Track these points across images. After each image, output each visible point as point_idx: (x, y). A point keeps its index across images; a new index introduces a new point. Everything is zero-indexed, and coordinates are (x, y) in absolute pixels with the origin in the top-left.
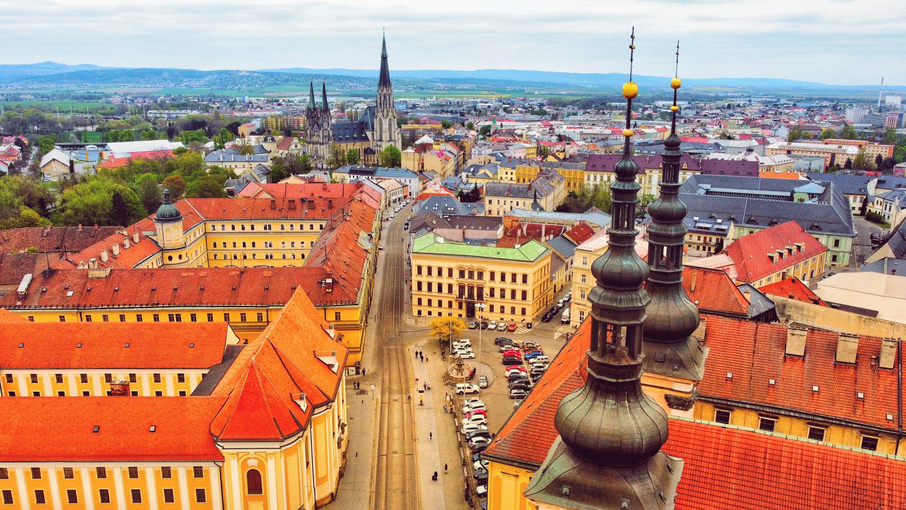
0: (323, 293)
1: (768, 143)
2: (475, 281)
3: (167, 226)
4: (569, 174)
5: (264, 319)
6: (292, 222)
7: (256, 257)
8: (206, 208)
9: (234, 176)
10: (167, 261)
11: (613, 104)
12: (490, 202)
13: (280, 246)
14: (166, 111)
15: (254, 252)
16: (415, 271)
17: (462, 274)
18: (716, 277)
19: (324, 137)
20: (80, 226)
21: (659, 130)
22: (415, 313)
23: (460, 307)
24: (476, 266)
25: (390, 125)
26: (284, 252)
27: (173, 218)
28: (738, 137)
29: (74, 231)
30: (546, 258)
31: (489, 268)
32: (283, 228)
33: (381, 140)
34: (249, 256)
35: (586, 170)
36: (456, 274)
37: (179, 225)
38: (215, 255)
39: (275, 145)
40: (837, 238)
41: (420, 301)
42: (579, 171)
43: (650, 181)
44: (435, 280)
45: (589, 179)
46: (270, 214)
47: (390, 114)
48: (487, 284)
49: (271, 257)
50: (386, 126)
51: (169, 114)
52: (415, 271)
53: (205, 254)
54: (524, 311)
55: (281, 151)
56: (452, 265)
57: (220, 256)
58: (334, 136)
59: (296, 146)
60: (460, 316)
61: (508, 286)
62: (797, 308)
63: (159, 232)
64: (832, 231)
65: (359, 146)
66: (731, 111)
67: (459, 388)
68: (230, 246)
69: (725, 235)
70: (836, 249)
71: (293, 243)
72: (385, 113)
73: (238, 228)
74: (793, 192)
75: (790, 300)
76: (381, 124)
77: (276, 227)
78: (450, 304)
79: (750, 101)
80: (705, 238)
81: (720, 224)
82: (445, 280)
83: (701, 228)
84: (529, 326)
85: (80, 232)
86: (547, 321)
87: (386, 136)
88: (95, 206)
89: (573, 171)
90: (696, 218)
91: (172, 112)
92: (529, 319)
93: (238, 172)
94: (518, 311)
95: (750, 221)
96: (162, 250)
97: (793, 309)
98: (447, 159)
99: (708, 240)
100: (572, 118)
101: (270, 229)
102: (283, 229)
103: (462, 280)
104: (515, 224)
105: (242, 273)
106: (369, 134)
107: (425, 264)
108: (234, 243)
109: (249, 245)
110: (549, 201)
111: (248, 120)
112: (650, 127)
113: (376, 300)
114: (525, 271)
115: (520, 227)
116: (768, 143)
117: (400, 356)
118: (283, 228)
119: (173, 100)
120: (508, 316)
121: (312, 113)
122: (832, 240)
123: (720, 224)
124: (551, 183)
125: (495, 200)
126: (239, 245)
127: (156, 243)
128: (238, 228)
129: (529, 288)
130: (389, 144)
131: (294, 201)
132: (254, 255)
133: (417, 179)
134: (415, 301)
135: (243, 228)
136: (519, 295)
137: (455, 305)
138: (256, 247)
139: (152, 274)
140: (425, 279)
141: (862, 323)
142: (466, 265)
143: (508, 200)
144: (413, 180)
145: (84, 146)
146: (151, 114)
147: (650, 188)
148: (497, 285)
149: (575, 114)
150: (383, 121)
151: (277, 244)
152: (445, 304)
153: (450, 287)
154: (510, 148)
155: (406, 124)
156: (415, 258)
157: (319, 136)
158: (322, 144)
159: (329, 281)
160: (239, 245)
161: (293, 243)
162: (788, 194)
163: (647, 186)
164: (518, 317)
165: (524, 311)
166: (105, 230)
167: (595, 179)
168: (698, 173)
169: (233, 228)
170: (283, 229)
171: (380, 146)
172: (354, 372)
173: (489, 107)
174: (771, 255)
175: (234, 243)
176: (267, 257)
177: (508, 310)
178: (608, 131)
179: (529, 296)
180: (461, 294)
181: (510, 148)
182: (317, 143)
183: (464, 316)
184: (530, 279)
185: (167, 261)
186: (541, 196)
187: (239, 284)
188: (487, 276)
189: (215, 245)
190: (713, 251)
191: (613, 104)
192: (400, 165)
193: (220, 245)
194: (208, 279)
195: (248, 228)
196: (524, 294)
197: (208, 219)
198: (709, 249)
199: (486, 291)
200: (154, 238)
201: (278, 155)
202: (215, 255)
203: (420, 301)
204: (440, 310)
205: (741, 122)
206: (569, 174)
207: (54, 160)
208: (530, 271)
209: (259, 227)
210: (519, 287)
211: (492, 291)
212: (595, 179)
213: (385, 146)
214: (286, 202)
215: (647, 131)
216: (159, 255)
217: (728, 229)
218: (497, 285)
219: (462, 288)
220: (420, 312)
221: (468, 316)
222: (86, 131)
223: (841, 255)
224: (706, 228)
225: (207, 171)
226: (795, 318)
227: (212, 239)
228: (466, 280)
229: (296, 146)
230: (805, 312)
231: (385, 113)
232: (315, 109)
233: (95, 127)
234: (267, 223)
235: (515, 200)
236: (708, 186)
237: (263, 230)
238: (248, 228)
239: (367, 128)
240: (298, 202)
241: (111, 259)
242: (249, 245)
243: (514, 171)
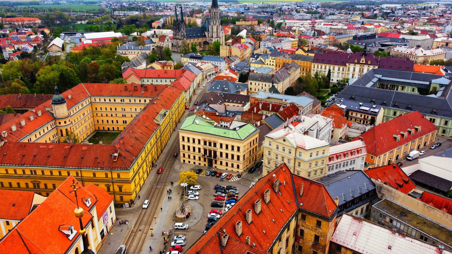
0: (111, 162)
1: (437, 37)
2: (212, 148)
3: (56, 106)
4: (304, 64)
5: (80, 175)
6: (135, 98)
7: (117, 115)
8: (91, 89)
9: (128, 60)
10: (58, 125)
11: (358, 6)
12: (251, 84)
13: (129, 110)
14: (123, 12)
15: (116, 113)
16: (181, 139)
17: (205, 143)
18: (317, 188)
19: (182, 36)
20: (35, 94)
21: (376, 26)
22: (182, 161)
23: (205, 161)
24: (213, 139)
25: (217, 29)
26: (132, 114)
27: (61, 102)
28: (419, 32)
29: (32, 97)
30: (256, 134)
31: (219, 141)
32: (130, 101)
33: (212, 37)
34: (114, 115)
35: (313, 62)
36: (202, 142)
37: (65, 105)
38: (97, 114)
39: (158, 39)
40: (447, 120)
41: (184, 155)
42: (309, 63)
43: (349, 70)
44: (191, 145)
45: (314, 67)
46: (124, 93)
47: (218, 23)
48: (219, 150)
49: (125, 116)
50: (215, 30)
51: (124, 14)
52: (181, 139)
53: (91, 114)
54: (238, 167)
55: (160, 43)
56: (200, 138)
57: (99, 114)
58: (186, 35)
59: (168, 40)
60: (205, 165)
61: (230, 152)
62: (388, 190)
63: (54, 109)
64: (444, 116)
65: (201, 40)
66: (424, 12)
67: (176, 226)
68: (104, 109)
69: (376, 116)
70: (445, 126)
71: (136, 109)
72: (215, 22)
73: (107, 101)
74: (430, 83)
75: (384, 185)
76: (212, 29)
77: (127, 100)
78: (200, 158)
79: (438, 4)
80: (365, 116)
81: (374, 108)
82: (197, 146)
83: (363, 110)
84: (239, 176)
85: (35, 97)
86: (251, 173)
87: (215, 35)
88: (50, 80)
89: (306, 62)
90: (361, 104)
91: (126, 12)
92: (241, 170)
93: (130, 57)
94: (235, 166)
95: (394, 106)
96: (55, 119)
97: (386, 191)
98: (246, 48)
99: (366, 117)
100: (331, 17)
101: (124, 101)
102: (130, 101)
103: (205, 146)
104: (257, 102)
105: (71, 147)
106: (206, 33)
107: (186, 136)
108: (106, 108)
109: (113, 109)
110: (281, 86)
111: (158, 18)
112: (371, 25)
113: (165, 151)
114: (239, 145)
115: (258, 104)
116: (437, 37)
117: (159, 194)
118: (130, 101)
119: (130, 4)
120: (230, 168)
121: (176, 23)
122: (443, 121)
123: (374, 108)
124: (289, 72)
125: (254, 83)
126: (109, 109)
127: (53, 114)
128: (107, 101)
129: (241, 154)
130: (217, 39)
131: (136, 87)
132: (116, 114)
133: (224, 62)
134: (182, 155)
135: (110, 101)
136: (235, 158)
137: (202, 159)
138: (117, 111)
139: (25, 146)
140: (186, 144)
141: (426, 208)
142: (208, 138)
143: (261, 83)
144: (222, 63)
145: (75, 34)
146: (116, 13)
147: (348, 74)
148: (224, 151)
149: (333, 14)
150: (214, 27)
151: (128, 109)
152: (197, 158)
153: (199, 149)
154: (282, 41)
155: (239, 21)
156: (182, 132)
157: (179, 35)
158: (180, 40)
159: (116, 155)
160: (109, 109)
161: (136, 109)
162: (428, 83)
163: (346, 72)
164: (235, 169)
165: (238, 167)
166: (47, 96)
167: (318, 68)
168: (376, 67)
169: (105, 100)
170: (130, 101)
171: (212, 40)
172: (128, 206)
173: (289, 8)
174: (395, 136)
175: (106, 108)
176: (123, 116)
177: (230, 165)
178: (346, 27)
179: (241, 158)
180: (205, 153)
181: (282, 41)
182: (178, 39)
183: (207, 165)
184: (241, 150)
185: (58, 125)
186: (279, 81)
187: (69, 154)
188: (218, 146)
189: (96, 109)
190: (369, 123)
191: (358, 6)
192: (219, 54)
193: (99, 109)
194: (53, 150)
195: (112, 101)
196: (238, 157)
197: (92, 95)
198: (367, 122)
199: (218, 154)
200: (52, 112)
201: (159, 45)
202: (97, 114)
203: (184, 155)
204: (195, 161)
205: (426, 21)
206: (304, 64)
207: (54, 44)
208: (241, 145)
209: (118, 100)
210: (236, 153)
211: (221, 154)
212: (318, 68)
213: (214, 40)
214: (133, 87)
215: (368, 27)
216: (53, 122)
217: (379, 111)
218: (224, 151)
219: (205, 150)
220: (184, 161)
221: (209, 165)
222: (81, 23)
223: (448, 130)
224: (366, 110)
225: (116, 57)
226: (387, 196)
227: (95, 106)
228: (207, 147)
229: (168, 40)
230: (393, 194)
231: (215, 22)
232: (177, 20)
233: (87, 21)
234: (122, 98)
235: (264, 83)
236: (380, 76)
237: (120, 102)
238: (112, 101)
239: (206, 30)
240: (139, 88)
241: (10, 135)
242: (113, 109)
243: (274, 61)
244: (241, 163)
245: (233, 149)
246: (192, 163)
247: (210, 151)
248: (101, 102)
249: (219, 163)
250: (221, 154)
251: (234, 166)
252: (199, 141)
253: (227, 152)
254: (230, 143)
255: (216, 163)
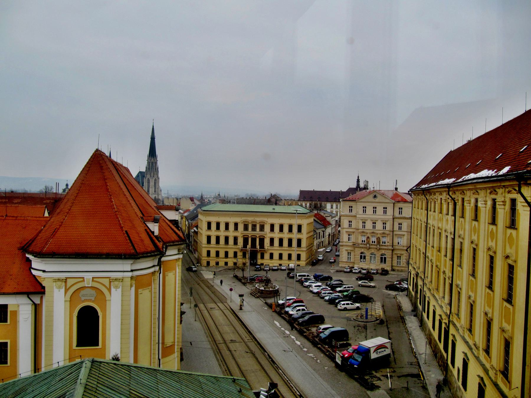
17: (246, 228)
48: (267, 234)
56: (238, 220)
61: (286, 235)
78: (235, 254)
82: (231, 233)
153: (236, 239)
165: (299, 257)
177: (285, 256)
184: (304, 229)
188: (267, 228)
210: (295, 236)
211: (272, 240)
218: (277, 235)
228: (250, 232)
244: (205, 247)
245: (218, 228)
246: (222, 264)
247: (254, 240)
248: (404, 215)
249: (267, 256)
250: (272, 240)
251: (229, 256)
252: (236, 225)
253: (227, 234)
254: (223, 220)
255: (262, 257)
